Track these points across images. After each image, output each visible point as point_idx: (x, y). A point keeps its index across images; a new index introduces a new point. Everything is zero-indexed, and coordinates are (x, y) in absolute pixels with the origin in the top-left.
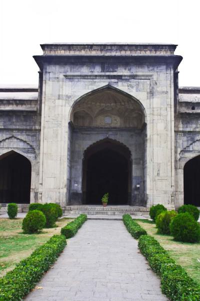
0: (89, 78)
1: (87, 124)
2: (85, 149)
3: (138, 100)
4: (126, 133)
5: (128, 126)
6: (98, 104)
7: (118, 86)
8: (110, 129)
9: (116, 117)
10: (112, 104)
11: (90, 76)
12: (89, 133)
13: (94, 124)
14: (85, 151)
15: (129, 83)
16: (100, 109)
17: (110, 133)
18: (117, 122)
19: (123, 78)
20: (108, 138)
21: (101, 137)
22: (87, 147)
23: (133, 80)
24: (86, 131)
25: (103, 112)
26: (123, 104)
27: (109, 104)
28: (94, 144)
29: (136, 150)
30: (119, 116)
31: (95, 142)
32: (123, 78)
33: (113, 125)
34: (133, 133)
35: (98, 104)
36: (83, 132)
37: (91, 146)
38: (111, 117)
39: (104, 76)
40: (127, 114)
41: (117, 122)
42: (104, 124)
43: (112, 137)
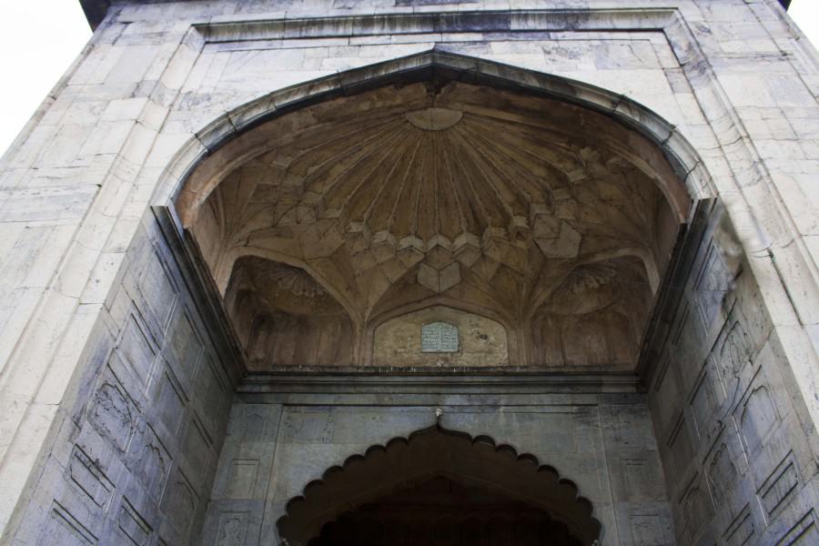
0: (328, 31)
1: (319, 351)
2: (296, 489)
3: (623, 100)
4: (546, 399)
5: (553, 359)
6: (383, 235)
7: (492, 53)
8: (446, 378)
9: (483, 322)
10: (461, 241)
11: (336, 22)
12: (330, 400)
13: (361, 355)
14: (294, 503)
15: (551, 44)
16: (396, 275)
17: (454, 400)
18: (493, 344)
19: (514, 25)
20: (438, 427)
21: (396, 423)
22: (307, 478)
23: (569, 35)
24: (311, 387)
25: (409, 297)
26: (520, 222)
27: (442, 241)
28: (353, 459)
29: (625, 497)
30: (497, 316)
31: (358, 448)
32: (514, 25)
33: (466, 360)
34: (589, 399)
35: (383, 235)
36: (294, 399)
37: (332, 472)
38: (456, 324)
39: (407, 20)
40: (542, 295)
41: (493, 344)
42: (416, 358)
43: (467, 423)
